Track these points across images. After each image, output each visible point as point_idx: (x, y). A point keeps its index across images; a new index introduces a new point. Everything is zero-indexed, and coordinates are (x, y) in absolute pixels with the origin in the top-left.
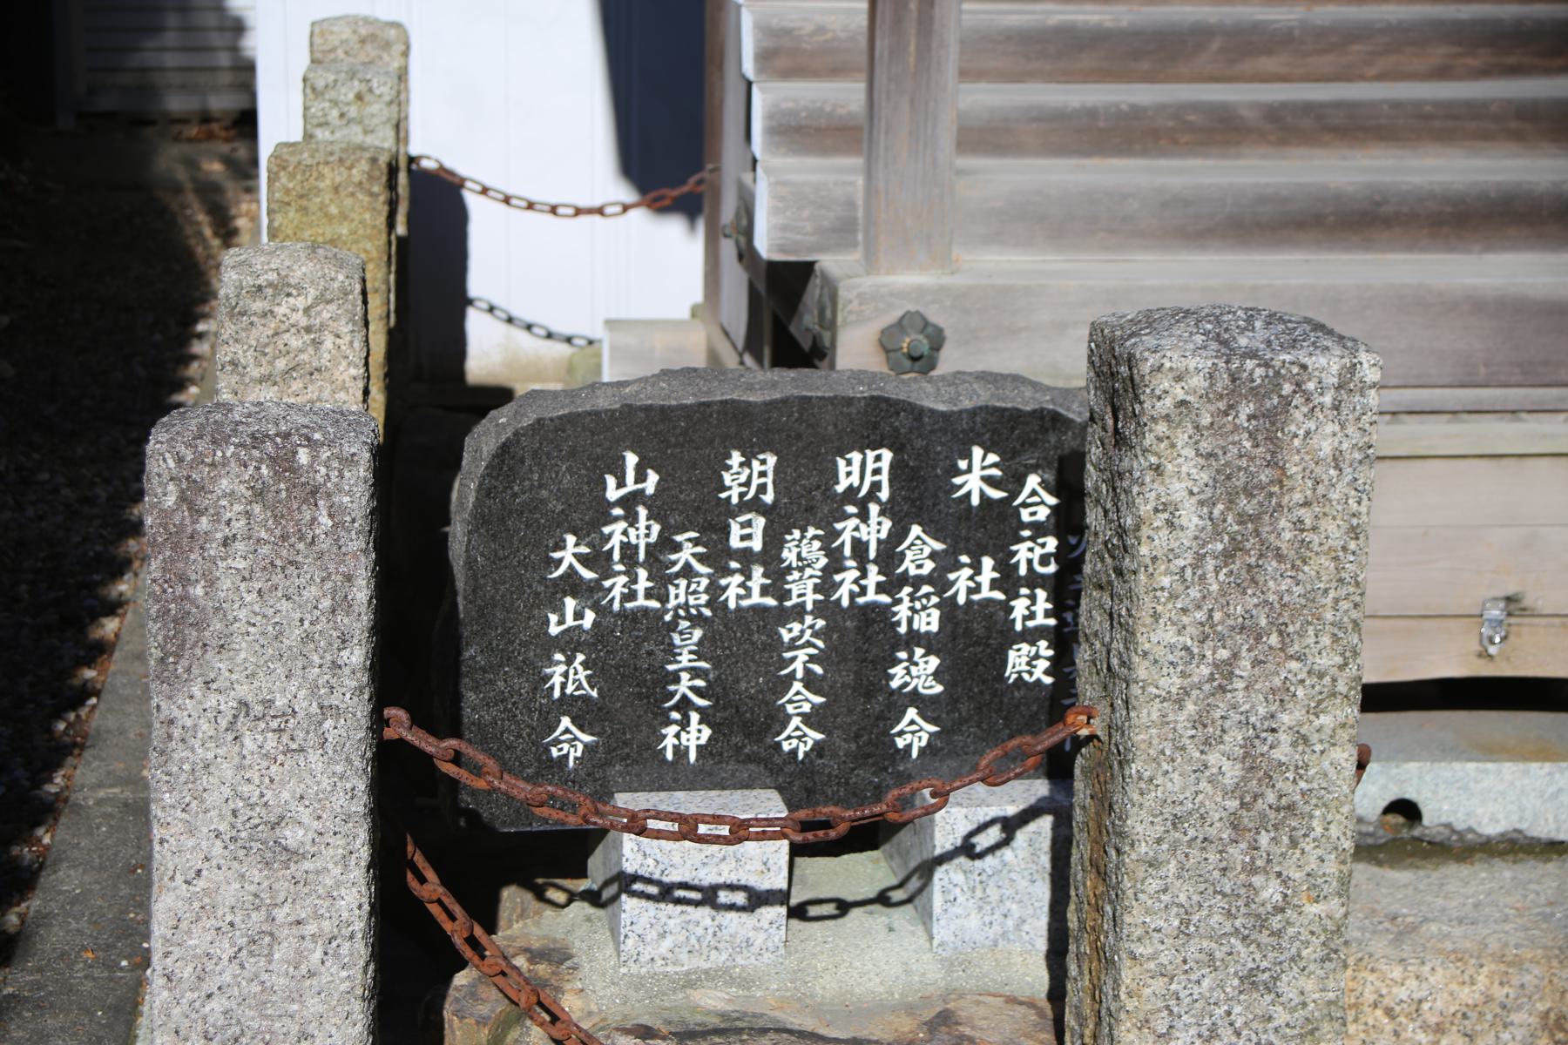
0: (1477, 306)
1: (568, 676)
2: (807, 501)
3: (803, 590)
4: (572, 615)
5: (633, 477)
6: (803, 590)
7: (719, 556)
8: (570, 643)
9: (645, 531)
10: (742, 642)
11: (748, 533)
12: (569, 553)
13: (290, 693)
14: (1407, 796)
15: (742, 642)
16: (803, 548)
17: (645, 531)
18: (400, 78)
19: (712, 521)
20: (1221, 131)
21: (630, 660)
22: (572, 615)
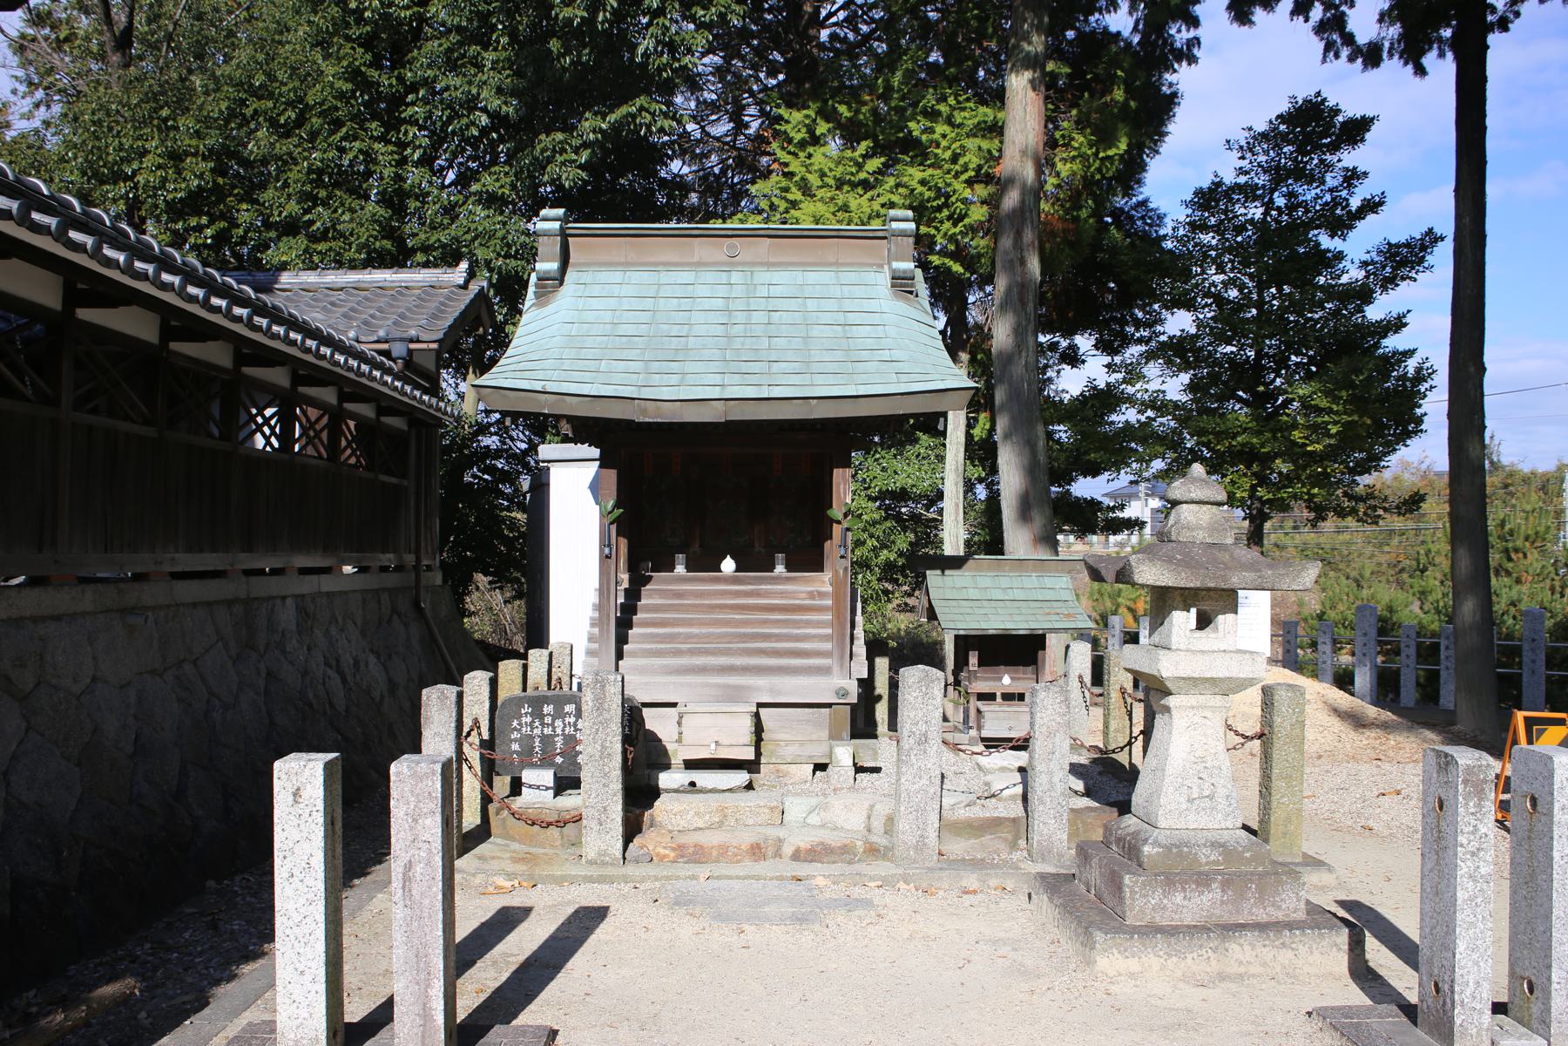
0: (719, 686)
1: (515, 747)
2: (559, 714)
3: (559, 731)
4: (515, 735)
5: (526, 709)
6: (559, 731)
7: (543, 724)
8: (515, 740)
9: (529, 719)
10: (547, 740)
11: (548, 720)
12: (515, 723)
13: (443, 731)
14: (1346, 971)
15: (547, 740)
16: (558, 723)
17: (529, 719)
18: (295, 795)
19: (541, 717)
20: (678, 653)
21: (527, 741)
22: (515, 735)
